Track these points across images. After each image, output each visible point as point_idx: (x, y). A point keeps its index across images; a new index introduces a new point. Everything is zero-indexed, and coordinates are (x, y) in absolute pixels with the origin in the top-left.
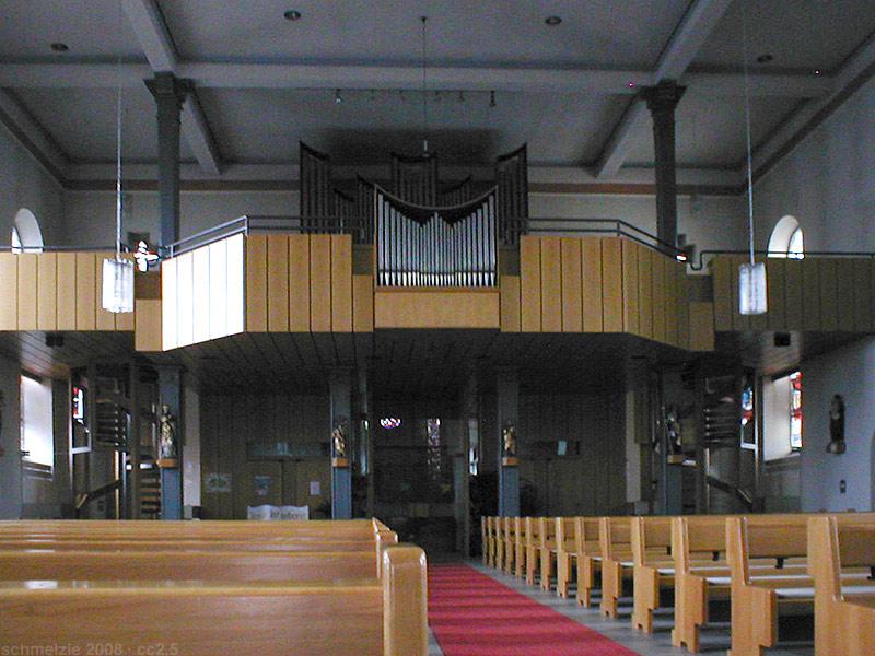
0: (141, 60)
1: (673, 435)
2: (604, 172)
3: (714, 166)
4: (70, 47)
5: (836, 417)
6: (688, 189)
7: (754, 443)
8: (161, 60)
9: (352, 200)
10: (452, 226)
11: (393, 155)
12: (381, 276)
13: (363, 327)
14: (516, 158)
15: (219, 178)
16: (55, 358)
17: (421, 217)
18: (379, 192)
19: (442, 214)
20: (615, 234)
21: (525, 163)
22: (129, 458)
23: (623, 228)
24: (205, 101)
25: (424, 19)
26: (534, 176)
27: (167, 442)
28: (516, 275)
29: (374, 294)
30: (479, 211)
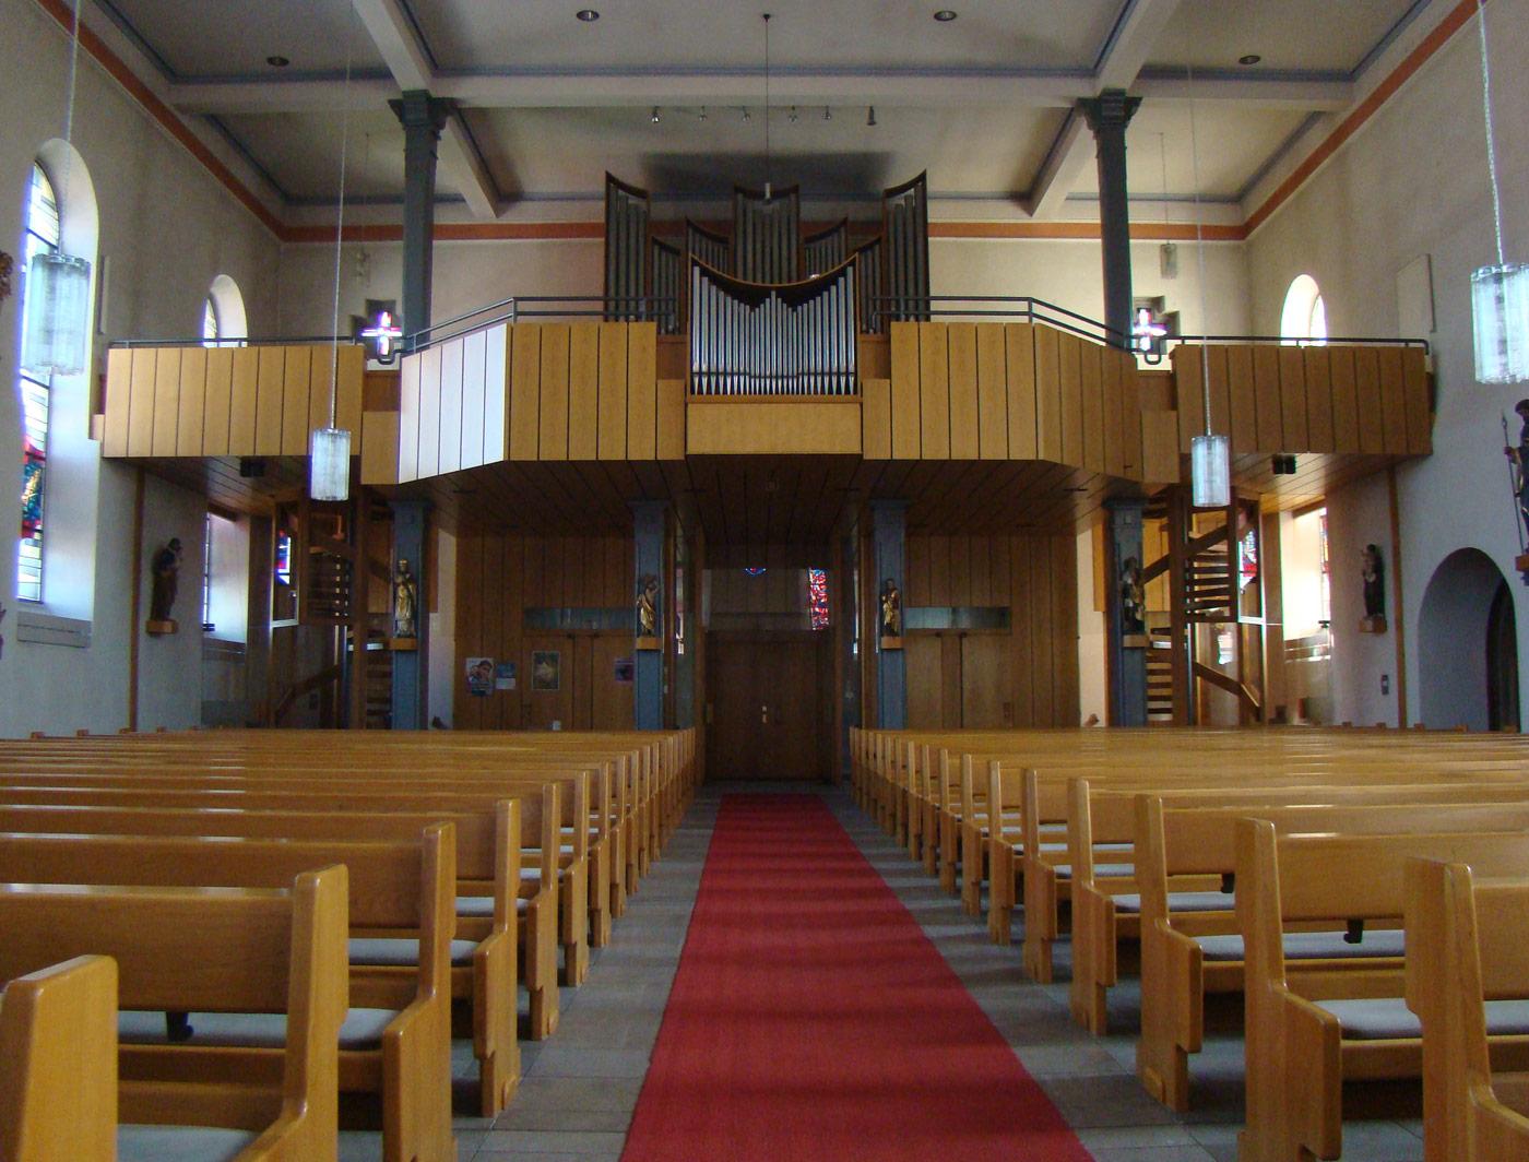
0: (379, 73)
1: (1131, 605)
2: (1038, 211)
3: (1191, 199)
4: (290, 59)
5: (1372, 579)
6: (1150, 232)
7: (1260, 615)
8: (411, 75)
9: (676, 252)
12: (696, 380)
13: (669, 452)
15: (495, 221)
16: (255, 490)
17: (752, 297)
18: (695, 263)
19: (781, 293)
20: (1025, 319)
21: (923, 197)
22: (351, 634)
23: (1037, 309)
24: (477, 126)
25: (767, 17)
26: (937, 213)
27: (402, 614)
28: (885, 378)
29: (686, 405)
30: (834, 289)
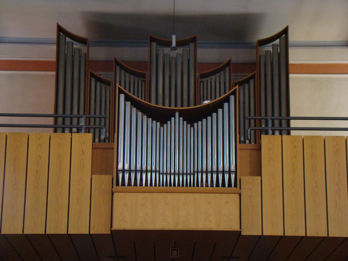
10: (192, 126)
11: (152, 40)
12: (121, 175)
14: (277, 41)
18: (121, 92)
19: (182, 114)
29: (113, 194)
